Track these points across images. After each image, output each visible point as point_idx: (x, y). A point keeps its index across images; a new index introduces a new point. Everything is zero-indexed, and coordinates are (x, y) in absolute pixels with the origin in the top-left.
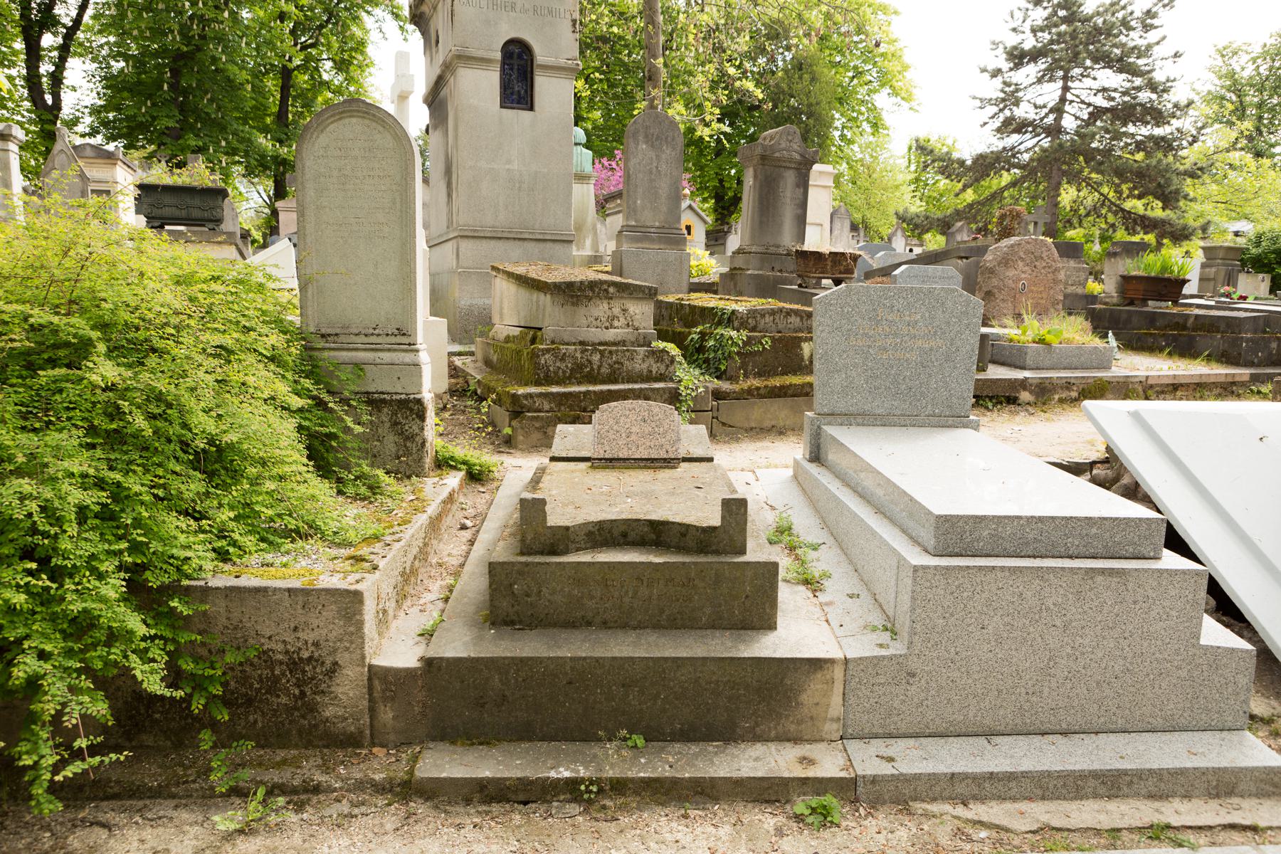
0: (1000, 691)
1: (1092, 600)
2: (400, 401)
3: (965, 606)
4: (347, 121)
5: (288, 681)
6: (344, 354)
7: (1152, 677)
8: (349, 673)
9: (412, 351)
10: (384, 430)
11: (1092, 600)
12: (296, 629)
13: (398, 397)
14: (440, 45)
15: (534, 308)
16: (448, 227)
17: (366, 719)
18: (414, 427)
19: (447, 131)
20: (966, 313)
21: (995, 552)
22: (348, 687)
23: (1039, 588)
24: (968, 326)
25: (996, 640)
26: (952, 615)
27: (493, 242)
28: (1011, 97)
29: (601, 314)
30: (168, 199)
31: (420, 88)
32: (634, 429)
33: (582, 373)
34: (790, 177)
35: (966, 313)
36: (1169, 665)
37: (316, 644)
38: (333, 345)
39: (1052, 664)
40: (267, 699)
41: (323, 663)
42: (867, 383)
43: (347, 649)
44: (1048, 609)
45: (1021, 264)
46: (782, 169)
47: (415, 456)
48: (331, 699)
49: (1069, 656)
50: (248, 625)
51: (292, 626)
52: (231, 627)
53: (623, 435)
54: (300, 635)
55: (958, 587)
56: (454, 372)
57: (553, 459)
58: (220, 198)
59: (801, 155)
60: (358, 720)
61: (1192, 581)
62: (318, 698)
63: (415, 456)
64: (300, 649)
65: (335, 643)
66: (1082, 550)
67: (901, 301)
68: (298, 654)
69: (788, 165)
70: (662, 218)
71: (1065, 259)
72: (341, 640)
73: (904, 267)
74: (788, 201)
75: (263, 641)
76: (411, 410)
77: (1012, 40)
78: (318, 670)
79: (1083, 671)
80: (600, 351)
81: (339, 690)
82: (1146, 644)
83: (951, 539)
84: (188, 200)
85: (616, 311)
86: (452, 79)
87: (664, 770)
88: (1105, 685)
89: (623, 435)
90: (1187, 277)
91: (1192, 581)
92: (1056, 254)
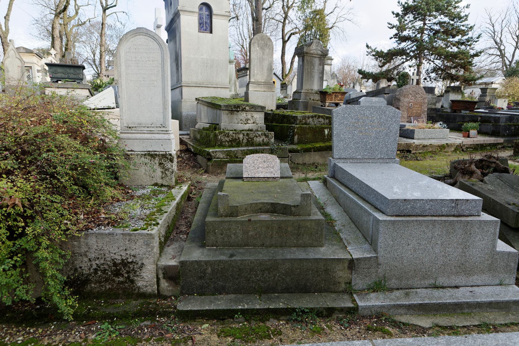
0: (415, 270)
1: (453, 233)
2: (163, 155)
3: (401, 236)
4: (138, 37)
5: (123, 271)
6: (139, 135)
7: (477, 264)
8: (149, 267)
9: (167, 134)
10: (156, 166)
11: (453, 233)
12: (126, 250)
13: (162, 153)
14: (172, 5)
15: (215, 116)
16: (177, 82)
17: (156, 286)
18: (169, 165)
19: (176, 42)
21: (413, 214)
22: (148, 273)
23: (431, 228)
24: (395, 122)
25: (414, 250)
26: (396, 240)
27: (196, 88)
28: (401, 28)
29: (243, 118)
30: (59, 70)
31: (164, 24)
33: (237, 143)
34: (317, 61)
35: (394, 116)
36: (483, 259)
37: (134, 256)
38: (134, 132)
39: (436, 259)
40: (114, 279)
41: (137, 264)
42: (354, 145)
43: (148, 258)
44: (435, 237)
45: (410, 96)
46: (314, 58)
47: (169, 177)
48: (141, 278)
49: (443, 256)
50: (106, 248)
51: (124, 248)
52: (98, 249)
53: (256, 168)
54: (128, 252)
55: (398, 228)
56: (182, 142)
57: (227, 178)
58: (82, 70)
59: (322, 52)
60: (152, 287)
61: (494, 225)
62: (135, 278)
63: (169, 177)
64: (128, 258)
65: (142, 255)
66: (448, 213)
68: (127, 260)
69: (316, 56)
70: (265, 78)
71: (428, 94)
72: (145, 254)
73: (363, 98)
74: (316, 71)
75: (112, 255)
76: (167, 158)
78: (135, 267)
79: (449, 262)
80: (243, 133)
81: (144, 275)
82: (474, 251)
83: (395, 209)
84: (68, 70)
85: (249, 116)
86: (178, 20)
87: (279, 305)
88: (458, 267)
89: (256, 168)
90: (450, 102)
91: (494, 225)
92: (425, 92)
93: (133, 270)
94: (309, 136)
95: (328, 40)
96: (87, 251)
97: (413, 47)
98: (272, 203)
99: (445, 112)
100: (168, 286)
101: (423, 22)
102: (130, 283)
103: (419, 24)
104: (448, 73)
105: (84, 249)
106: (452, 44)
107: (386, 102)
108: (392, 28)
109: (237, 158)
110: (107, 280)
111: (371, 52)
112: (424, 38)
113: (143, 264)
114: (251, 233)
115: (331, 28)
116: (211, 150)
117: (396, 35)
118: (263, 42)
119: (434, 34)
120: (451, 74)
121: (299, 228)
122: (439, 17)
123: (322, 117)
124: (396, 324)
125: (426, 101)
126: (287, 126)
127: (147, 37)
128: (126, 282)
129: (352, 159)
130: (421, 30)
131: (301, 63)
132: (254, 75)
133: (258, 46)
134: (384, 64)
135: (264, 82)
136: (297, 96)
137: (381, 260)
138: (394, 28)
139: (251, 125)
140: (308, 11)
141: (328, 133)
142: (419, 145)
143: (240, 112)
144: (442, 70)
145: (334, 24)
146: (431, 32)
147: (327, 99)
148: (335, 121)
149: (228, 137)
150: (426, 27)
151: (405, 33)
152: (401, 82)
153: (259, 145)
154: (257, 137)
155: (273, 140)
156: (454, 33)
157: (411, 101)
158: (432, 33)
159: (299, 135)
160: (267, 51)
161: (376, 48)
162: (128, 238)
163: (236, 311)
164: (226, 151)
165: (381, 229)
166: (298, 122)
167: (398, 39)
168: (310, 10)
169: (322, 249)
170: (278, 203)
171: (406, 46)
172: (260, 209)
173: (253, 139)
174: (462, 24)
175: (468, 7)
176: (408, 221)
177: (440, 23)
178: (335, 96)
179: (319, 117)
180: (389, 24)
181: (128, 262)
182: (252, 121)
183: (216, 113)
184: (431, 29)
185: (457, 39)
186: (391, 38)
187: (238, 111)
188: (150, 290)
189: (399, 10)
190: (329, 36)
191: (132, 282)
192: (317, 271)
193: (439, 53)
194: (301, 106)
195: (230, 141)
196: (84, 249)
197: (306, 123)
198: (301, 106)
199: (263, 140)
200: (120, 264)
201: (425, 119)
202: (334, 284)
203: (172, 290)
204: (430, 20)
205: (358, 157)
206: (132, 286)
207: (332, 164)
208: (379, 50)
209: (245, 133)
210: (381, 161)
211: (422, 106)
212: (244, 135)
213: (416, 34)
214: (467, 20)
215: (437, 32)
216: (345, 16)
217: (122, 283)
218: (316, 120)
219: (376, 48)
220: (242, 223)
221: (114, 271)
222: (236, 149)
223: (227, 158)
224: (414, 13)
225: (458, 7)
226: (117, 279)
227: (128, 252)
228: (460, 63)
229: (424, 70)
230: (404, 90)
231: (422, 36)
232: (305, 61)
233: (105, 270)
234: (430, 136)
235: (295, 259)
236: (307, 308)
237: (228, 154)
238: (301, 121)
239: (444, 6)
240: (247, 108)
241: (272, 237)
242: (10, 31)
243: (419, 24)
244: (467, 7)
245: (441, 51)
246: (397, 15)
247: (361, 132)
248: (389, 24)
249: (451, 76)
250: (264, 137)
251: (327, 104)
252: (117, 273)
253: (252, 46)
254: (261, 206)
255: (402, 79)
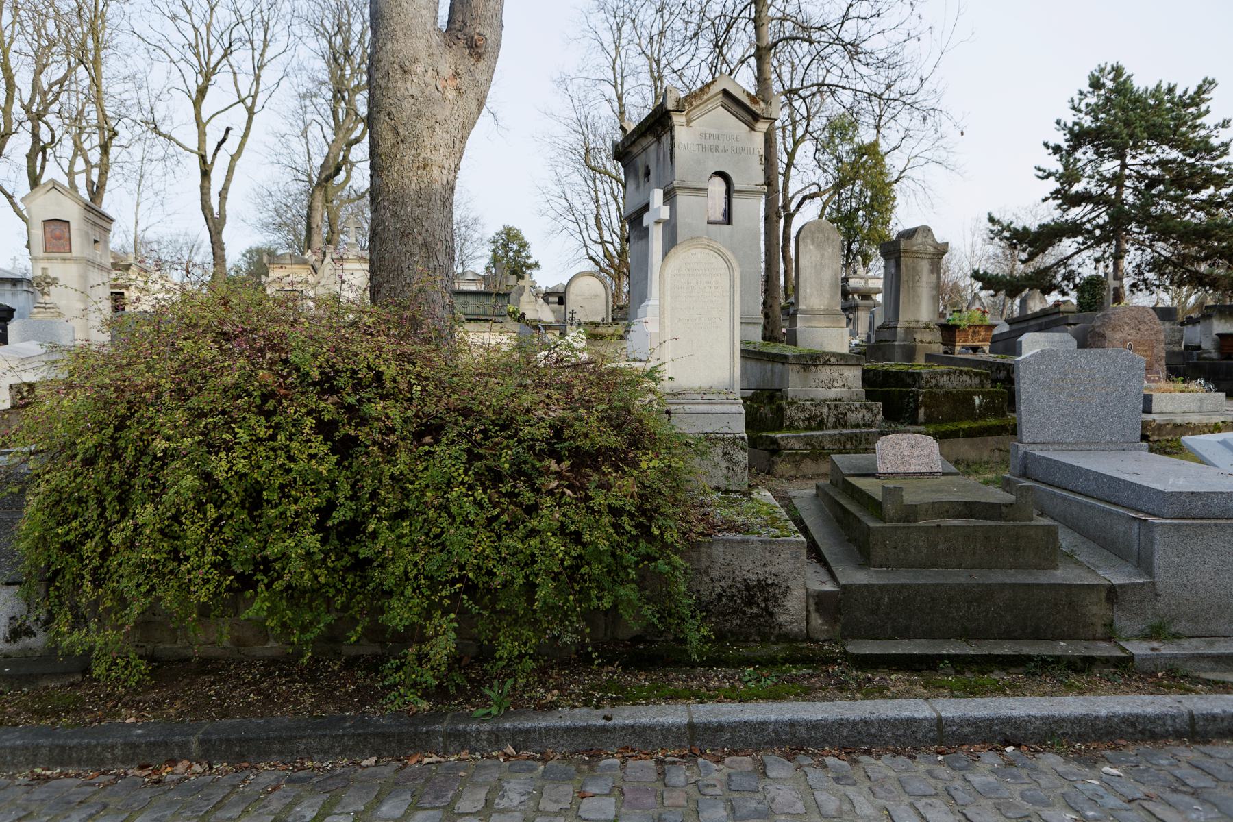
20: (1132, 367)
24: (1134, 376)
26: (1183, 555)
28: (1070, 176)
29: (825, 377)
32: (906, 453)
34: (925, 266)
35: (1132, 367)
37: (776, 575)
45: (1127, 328)
67: (1082, 360)
74: (924, 284)
77: (1069, 118)
81: (789, 604)
85: (836, 375)
93: (774, 596)
94: (945, 408)
95: (893, 207)
96: (709, 567)
97: (1098, 216)
98: (966, 503)
99: (1205, 359)
100: (822, 624)
101: (1118, 162)
102: (767, 617)
103: (1110, 166)
104: (1189, 271)
105: (705, 563)
106: (1193, 207)
107: (1075, 342)
108: (1047, 177)
109: (823, 449)
110: (734, 611)
111: (1001, 232)
112: (1124, 197)
113: (788, 587)
114: (940, 547)
115: (897, 181)
116: (778, 435)
117: (1057, 192)
118: (821, 235)
119: (1146, 185)
120: (1197, 272)
121: (1017, 539)
122: (1159, 151)
123: (967, 373)
124: (1198, 680)
125: (1162, 337)
126: (900, 392)
127: (707, 251)
128: (762, 616)
129: (1058, 443)
130: (1117, 180)
131: (893, 270)
132: (805, 298)
133: (813, 244)
134: (1032, 257)
135: (824, 310)
136: (886, 335)
137: (1161, 588)
138: (1052, 179)
139: (838, 390)
140: (844, 149)
141: (981, 403)
142: (1165, 425)
143: (820, 367)
144: (1175, 265)
145: (902, 172)
146: (1140, 182)
147: (958, 339)
148: (1023, 378)
149: (803, 411)
150: (1127, 172)
151: (1078, 187)
152: (1086, 296)
153: (857, 426)
154: (852, 411)
155: (880, 417)
156: (1199, 182)
157: (1129, 337)
158: (1143, 184)
159: (927, 407)
160: (830, 250)
161: (1011, 223)
162: (768, 547)
163: (941, 658)
164: (805, 436)
165: (1157, 537)
166: (923, 383)
167: (1060, 201)
168: (848, 147)
169: (1058, 572)
170: (976, 502)
171: (1082, 214)
172: (947, 512)
173: (845, 415)
174: (1215, 163)
175: (1225, 124)
176: (1201, 525)
177: (1162, 163)
178: (974, 332)
179: (961, 372)
180: (1039, 169)
181: (767, 585)
182: (840, 383)
183: (772, 370)
184: (1141, 176)
185: (1204, 194)
186: (1045, 200)
187: (816, 366)
188: (796, 629)
189: (1061, 139)
190: (895, 197)
191: (771, 614)
192: (1056, 605)
193: (1163, 228)
194: (898, 354)
195: (807, 419)
196: (705, 563)
197: (937, 386)
198: (898, 354)
199: (864, 416)
200: (754, 587)
201: (1163, 374)
202: (1084, 627)
203: (828, 631)
204: (1134, 157)
205: (1068, 441)
206: (770, 621)
207: (1020, 453)
208: (1018, 225)
209: (832, 404)
210: (1113, 446)
211: (1153, 347)
212: (830, 408)
213: (1105, 187)
214: (1227, 154)
215: (1153, 182)
216: (928, 154)
217: (757, 616)
218: (955, 380)
219: (1011, 223)
220: (927, 529)
221: (746, 597)
222: (821, 433)
223: (806, 449)
224: (1096, 143)
225: (1202, 126)
226: (748, 611)
227: (768, 569)
228: (1219, 249)
229: (1131, 266)
230: (1113, 317)
231: (1119, 194)
232: (903, 267)
233: (733, 596)
234: (1184, 408)
235: (1020, 584)
236: (1051, 656)
237: (808, 441)
238: (927, 382)
239: (1168, 126)
240: (832, 359)
241: (974, 553)
242: (228, 220)
243: (1110, 166)
244: (1223, 126)
245: (1171, 224)
246: (1057, 149)
247: (1072, 396)
248: (1039, 169)
249: (1197, 278)
250: (865, 411)
251: (958, 349)
252: (750, 602)
253: (801, 243)
254: (947, 506)
255: (1089, 291)
